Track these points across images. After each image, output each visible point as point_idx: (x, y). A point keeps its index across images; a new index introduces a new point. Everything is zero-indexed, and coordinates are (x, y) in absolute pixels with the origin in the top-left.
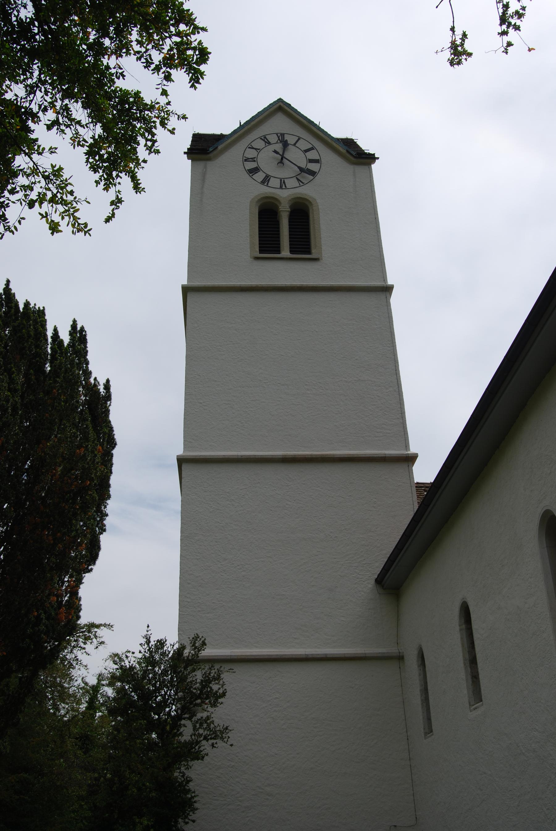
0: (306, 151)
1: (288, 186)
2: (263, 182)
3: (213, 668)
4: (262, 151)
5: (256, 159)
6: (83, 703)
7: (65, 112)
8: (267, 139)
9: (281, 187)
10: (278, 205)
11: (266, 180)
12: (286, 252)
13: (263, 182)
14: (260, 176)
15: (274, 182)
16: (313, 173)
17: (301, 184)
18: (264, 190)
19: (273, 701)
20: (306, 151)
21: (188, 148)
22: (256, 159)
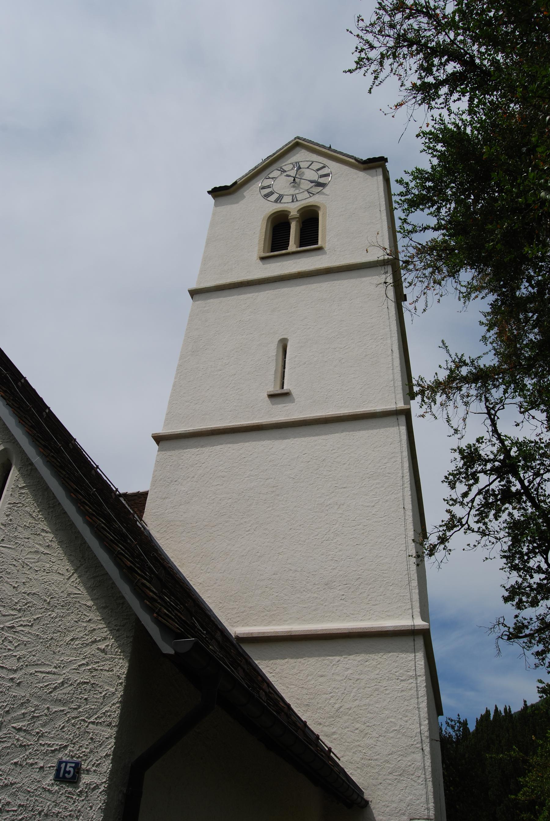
0: (318, 170)
1: (298, 199)
2: (276, 201)
3: (525, 440)
4: (278, 179)
5: (271, 186)
6: (489, 512)
7: (455, 129)
8: (283, 169)
9: (293, 201)
10: (317, 209)
11: (279, 200)
12: (292, 246)
13: (276, 201)
14: (273, 197)
15: (286, 199)
16: (323, 185)
17: (311, 195)
18: (278, 207)
19: (530, 446)
20: (318, 170)
21: (387, 162)
22: (271, 186)
